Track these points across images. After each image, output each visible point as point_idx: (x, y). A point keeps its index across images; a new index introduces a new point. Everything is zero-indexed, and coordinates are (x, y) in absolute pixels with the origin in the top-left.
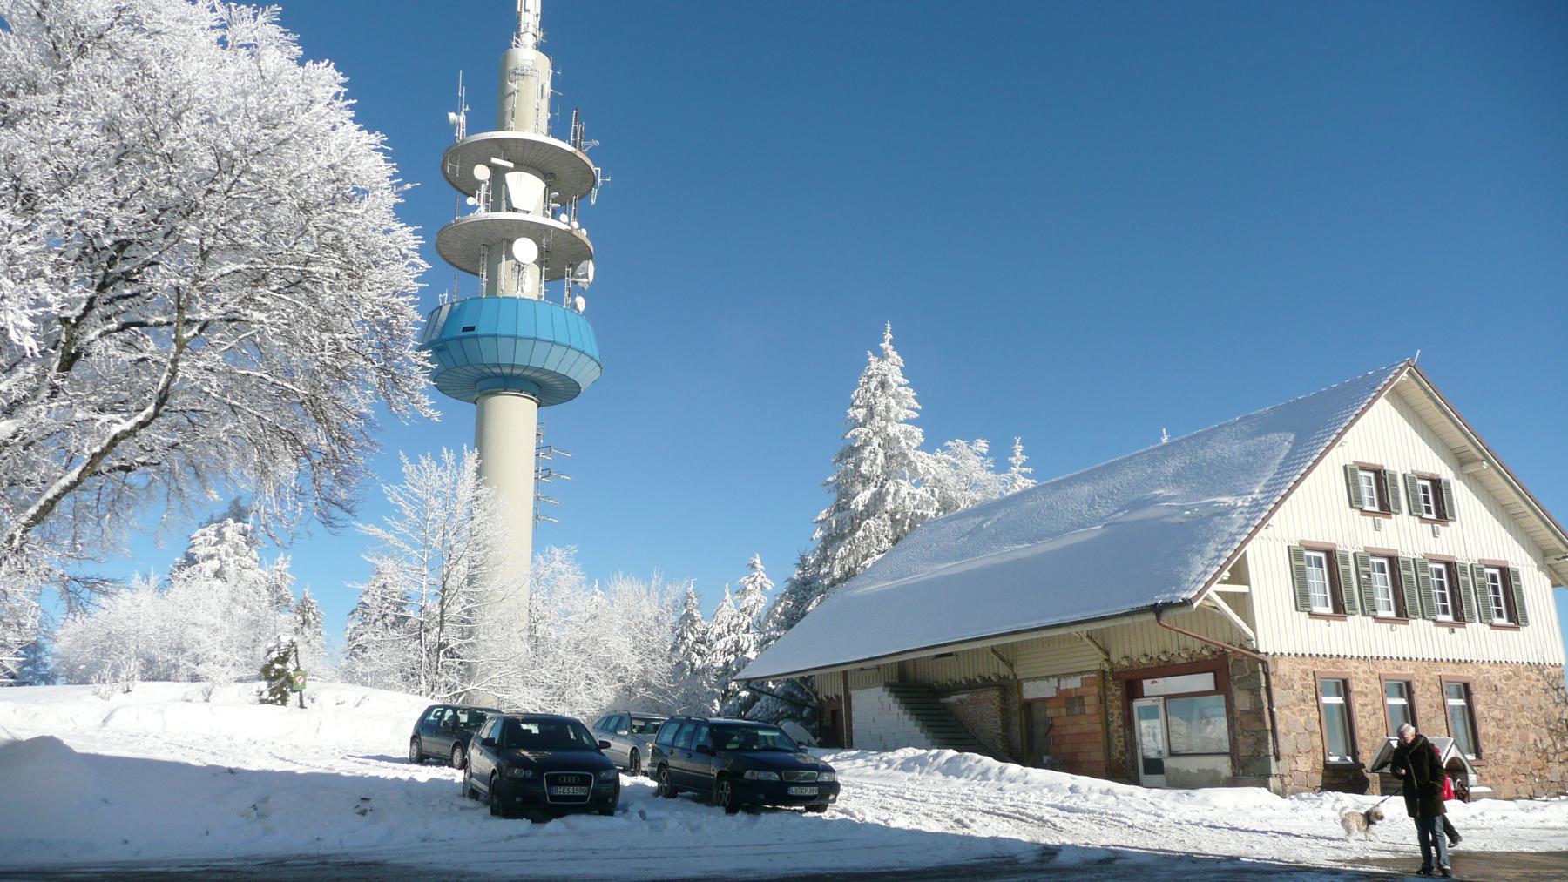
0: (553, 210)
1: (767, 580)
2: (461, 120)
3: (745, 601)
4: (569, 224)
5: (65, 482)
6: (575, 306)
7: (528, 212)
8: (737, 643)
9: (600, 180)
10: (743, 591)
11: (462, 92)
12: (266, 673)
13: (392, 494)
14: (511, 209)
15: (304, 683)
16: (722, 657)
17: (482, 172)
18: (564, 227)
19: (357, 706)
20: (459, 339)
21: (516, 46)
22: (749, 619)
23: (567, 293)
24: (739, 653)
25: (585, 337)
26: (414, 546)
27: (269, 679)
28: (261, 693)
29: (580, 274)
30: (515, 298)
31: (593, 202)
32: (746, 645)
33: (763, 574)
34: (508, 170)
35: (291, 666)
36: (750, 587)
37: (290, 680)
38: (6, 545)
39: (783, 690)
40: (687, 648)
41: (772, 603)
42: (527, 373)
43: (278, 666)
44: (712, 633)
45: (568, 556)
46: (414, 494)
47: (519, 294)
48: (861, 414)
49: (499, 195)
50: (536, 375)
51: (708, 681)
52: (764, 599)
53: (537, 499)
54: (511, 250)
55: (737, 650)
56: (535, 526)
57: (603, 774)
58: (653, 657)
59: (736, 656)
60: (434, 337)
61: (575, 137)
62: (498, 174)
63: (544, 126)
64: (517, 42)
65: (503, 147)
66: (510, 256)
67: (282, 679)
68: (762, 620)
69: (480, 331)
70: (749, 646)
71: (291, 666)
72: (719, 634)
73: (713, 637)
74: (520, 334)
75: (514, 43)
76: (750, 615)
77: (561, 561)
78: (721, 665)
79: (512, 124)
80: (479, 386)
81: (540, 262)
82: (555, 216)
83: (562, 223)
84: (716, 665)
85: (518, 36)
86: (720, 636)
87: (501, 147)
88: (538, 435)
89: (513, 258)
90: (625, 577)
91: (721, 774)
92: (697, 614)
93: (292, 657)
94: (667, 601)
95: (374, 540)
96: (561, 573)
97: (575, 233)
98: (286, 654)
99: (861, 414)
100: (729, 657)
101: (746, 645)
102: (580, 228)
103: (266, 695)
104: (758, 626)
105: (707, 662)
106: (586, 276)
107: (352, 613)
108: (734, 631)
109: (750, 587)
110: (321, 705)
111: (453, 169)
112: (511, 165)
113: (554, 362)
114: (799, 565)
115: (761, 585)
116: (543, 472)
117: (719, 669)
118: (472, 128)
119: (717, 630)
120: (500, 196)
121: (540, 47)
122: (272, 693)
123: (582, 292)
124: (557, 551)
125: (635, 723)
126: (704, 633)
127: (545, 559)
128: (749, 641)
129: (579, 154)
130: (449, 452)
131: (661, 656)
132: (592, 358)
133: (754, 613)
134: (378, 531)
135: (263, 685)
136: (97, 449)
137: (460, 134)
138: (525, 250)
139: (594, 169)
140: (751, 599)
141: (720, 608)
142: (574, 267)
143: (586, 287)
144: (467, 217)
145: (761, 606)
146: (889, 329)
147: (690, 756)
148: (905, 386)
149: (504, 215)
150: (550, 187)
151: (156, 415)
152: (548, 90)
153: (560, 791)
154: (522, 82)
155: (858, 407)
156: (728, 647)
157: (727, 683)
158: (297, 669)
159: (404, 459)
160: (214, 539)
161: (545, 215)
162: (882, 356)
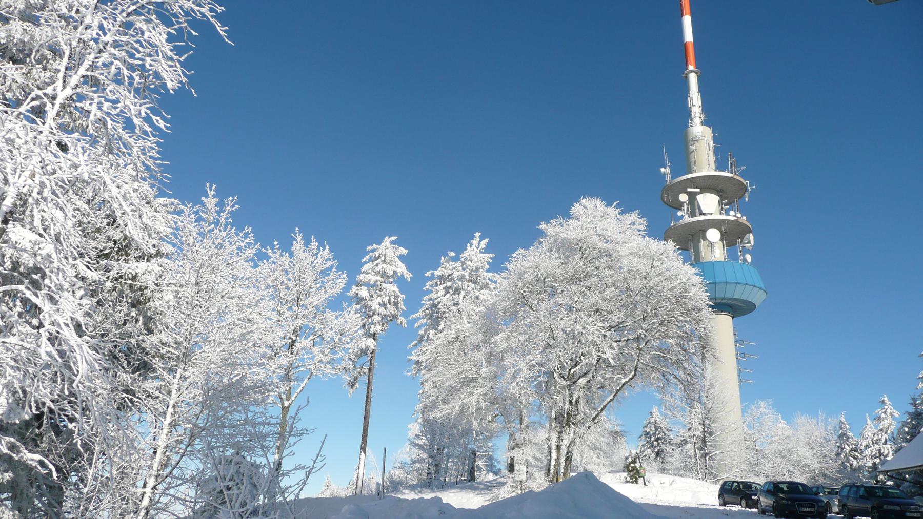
0: (725, 210)
1: (894, 411)
2: (668, 171)
3: (881, 424)
4: (735, 216)
5: (609, 399)
6: (745, 260)
7: (711, 214)
9: (749, 188)
10: (879, 419)
11: (666, 157)
12: (627, 468)
14: (702, 214)
15: (645, 473)
16: (871, 460)
17: (683, 198)
18: (733, 218)
19: (671, 484)
21: (691, 126)
23: (740, 253)
24: (882, 458)
25: (755, 277)
27: (629, 471)
28: (626, 478)
29: (746, 242)
30: (711, 262)
32: (886, 452)
35: (638, 465)
37: (638, 472)
38: (178, 376)
39: (912, 479)
40: (846, 454)
43: (632, 465)
44: (862, 445)
45: (769, 405)
47: (713, 259)
49: (694, 208)
50: (729, 302)
51: (864, 476)
52: (894, 423)
54: (706, 236)
55: (880, 455)
56: (741, 387)
57: (820, 504)
58: (826, 459)
59: (881, 459)
61: (731, 167)
62: (692, 197)
63: (713, 165)
64: (691, 123)
65: (693, 182)
66: (705, 239)
67: (635, 471)
68: (895, 436)
70: (889, 453)
71: (638, 465)
72: (867, 445)
73: (863, 448)
74: (717, 281)
75: (690, 124)
76: (886, 433)
77: (765, 408)
78: (871, 465)
79: (696, 168)
81: (722, 240)
82: (727, 213)
83: (732, 216)
84: (867, 465)
85: (691, 120)
86: (867, 447)
88: (734, 334)
89: (707, 240)
90: (802, 415)
91: (873, 507)
92: (850, 434)
93: (638, 461)
94: (830, 427)
96: (765, 414)
97: (740, 221)
98: (635, 459)
100: (875, 460)
101: (886, 452)
102: (742, 216)
103: (628, 479)
105: (861, 463)
106: (749, 242)
107: (640, 437)
108: (877, 443)
109: (883, 415)
110: (653, 484)
111: (667, 198)
112: (698, 190)
114: (912, 404)
115: (891, 414)
116: (741, 355)
117: (870, 467)
118: (674, 175)
119: (865, 443)
120: (694, 206)
121: (704, 123)
122: (631, 478)
123: (748, 252)
124: (762, 403)
125: (826, 490)
126: (856, 445)
127: (756, 407)
128: (888, 449)
131: (831, 459)
132: (760, 289)
133: (889, 432)
135: (626, 474)
136: (618, 388)
137: (668, 179)
138: (713, 235)
139: (745, 183)
140: (885, 423)
141: (864, 429)
142: (742, 238)
143: (750, 248)
145: (893, 427)
147: (857, 500)
150: (722, 198)
151: (635, 375)
152: (712, 145)
153: (803, 509)
154: (697, 144)
156: (874, 453)
157: (877, 476)
158: (641, 466)
161: (721, 214)
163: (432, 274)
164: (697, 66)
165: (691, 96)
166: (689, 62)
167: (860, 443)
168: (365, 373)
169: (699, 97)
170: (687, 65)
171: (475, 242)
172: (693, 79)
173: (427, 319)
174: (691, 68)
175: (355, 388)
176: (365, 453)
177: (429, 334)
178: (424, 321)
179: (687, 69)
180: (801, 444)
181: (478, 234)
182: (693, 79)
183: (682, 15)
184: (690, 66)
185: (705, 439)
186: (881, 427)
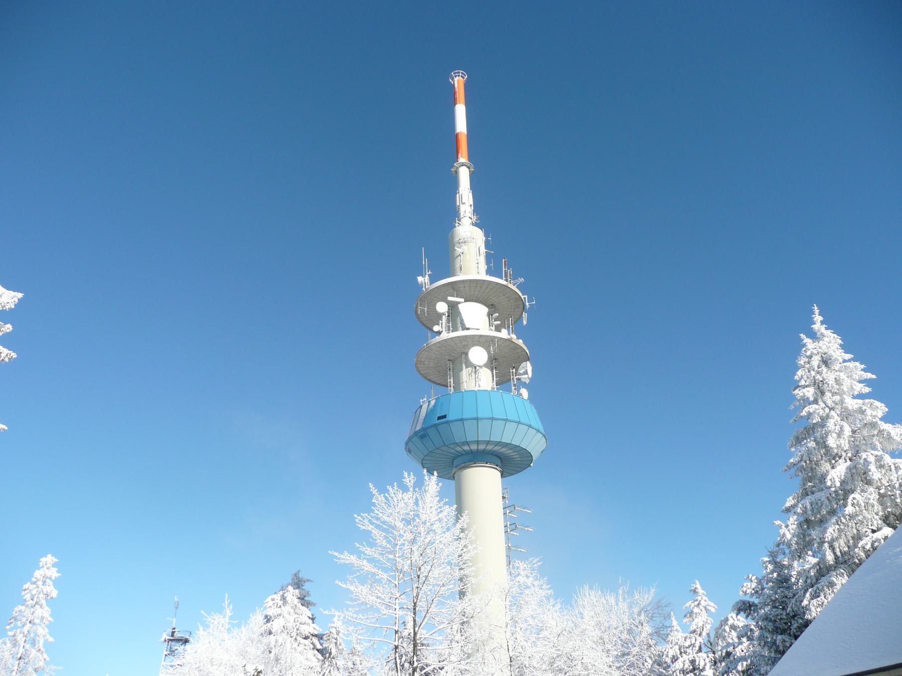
2: (426, 281)
3: (694, 623)
8: (693, 662)
9: (527, 304)
13: (363, 522)
14: (465, 328)
20: (435, 426)
22: (700, 640)
25: (531, 416)
26: (385, 570)
31: (525, 323)
32: (702, 664)
33: (705, 598)
34: (459, 303)
36: (696, 610)
41: (718, 624)
42: (490, 447)
44: (667, 656)
46: (384, 522)
47: (477, 388)
48: (810, 392)
50: (497, 448)
52: (710, 620)
53: (509, 548)
60: (418, 428)
63: (483, 267)
65: (454, 288)
68: (712, 640)
69: (449, 418)
70: (705, 665)
73: (668, 660)
74: (480, 416)
75: (457, 224)
76: (700, 635)
83: (504, 334)
85: (459, 220)
87: (453, 289)
88: (504, 498)
95: (348, 569)
96: (527, 587)
99: (810, 392)
101: (702, 664)
104: (709, 645)
106: (526, 373)
111: (422, 311)
112: (463, 300)
113: (509, 435)
115: (705, 608)
116: (511, 527)
123: (525, 385)
129: (511, 286)
130: (409, 475)
132: (538, 431)
133: (704, 634)
134: (353, 559)
138: (478, 355)
139: (522, 297)
140: (699, 621)
142: (517, 368)
143: (527, 381)
144: (434, 339)
145: (709, 626)
146: (817, 311)
148: (849, 361)
149: (460, 333)
152: (483, 250)
155: (805, 387)
159: (375, 491)
160: (281, 603)
162: (814, 336)
165: (460, 193)
166: (460, 155)
167: (665, 653)
170: (457, 157)
172: (464, 175)
174: (463, 159)
180: (590, 643)
182: (464, 175)
183: (455, 104)
185: (415, 640)
186: (695, 627)
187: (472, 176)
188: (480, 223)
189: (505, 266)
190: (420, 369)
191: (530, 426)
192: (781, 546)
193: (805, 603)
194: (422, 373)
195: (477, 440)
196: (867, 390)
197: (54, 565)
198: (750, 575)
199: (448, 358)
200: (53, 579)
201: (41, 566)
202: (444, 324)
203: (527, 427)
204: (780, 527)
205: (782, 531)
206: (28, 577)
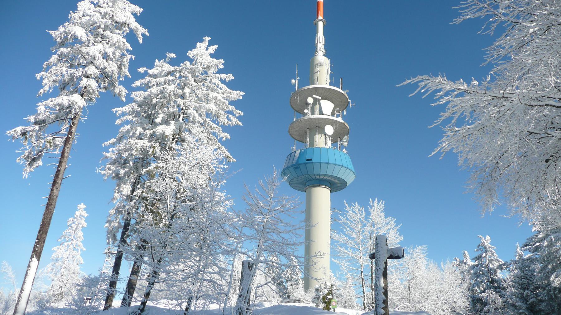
2: (296, 83)
9: (350, 105)
17: (310, 100)
20: (305, 163)
29: (344, 141)
30: (319, 148)
42: (325, 178)
50: (329, 178)
63: (328, 81)
69: (314, 161)
74: (330, 162)
80: (307, 184)
85: (317, 52)
87: (316, 91)
118: (301, 84)
132: (351, 171)
143: (346, 146)
159: (346, 205)
163: (146, 72)
164: (324, 17)
165: (319, 37)
166: (319, 14)
168: (56, 146)
169: (324, 39)
171: (204, 45)
172: (321, 25)
173: (133, 117)
174: (321, 17)
175: (35, 165)
176: (38, 260)
177: (136, 130)
178: (130, 118)
179: (318, 18)
181: (207, 39)
182: (321, 25)
184: (320, 16)
187: (324, 26)
188: (326, 55)
189: (341, 82)
190: (290, 130)
191: (347, 168)
192: (480, 247)
193: (551, 279)
194: (290, 132)
195: (319, 173)
196: (441, 151)
197: (85, 209)
198: (457, 258)
199: (308, 127)
200: (85, 217)
201: (78, 209)
202: (310, 109)
203: (327, 164)
204: (481, 238)
205: (482, 241)
206: (73, 215)
